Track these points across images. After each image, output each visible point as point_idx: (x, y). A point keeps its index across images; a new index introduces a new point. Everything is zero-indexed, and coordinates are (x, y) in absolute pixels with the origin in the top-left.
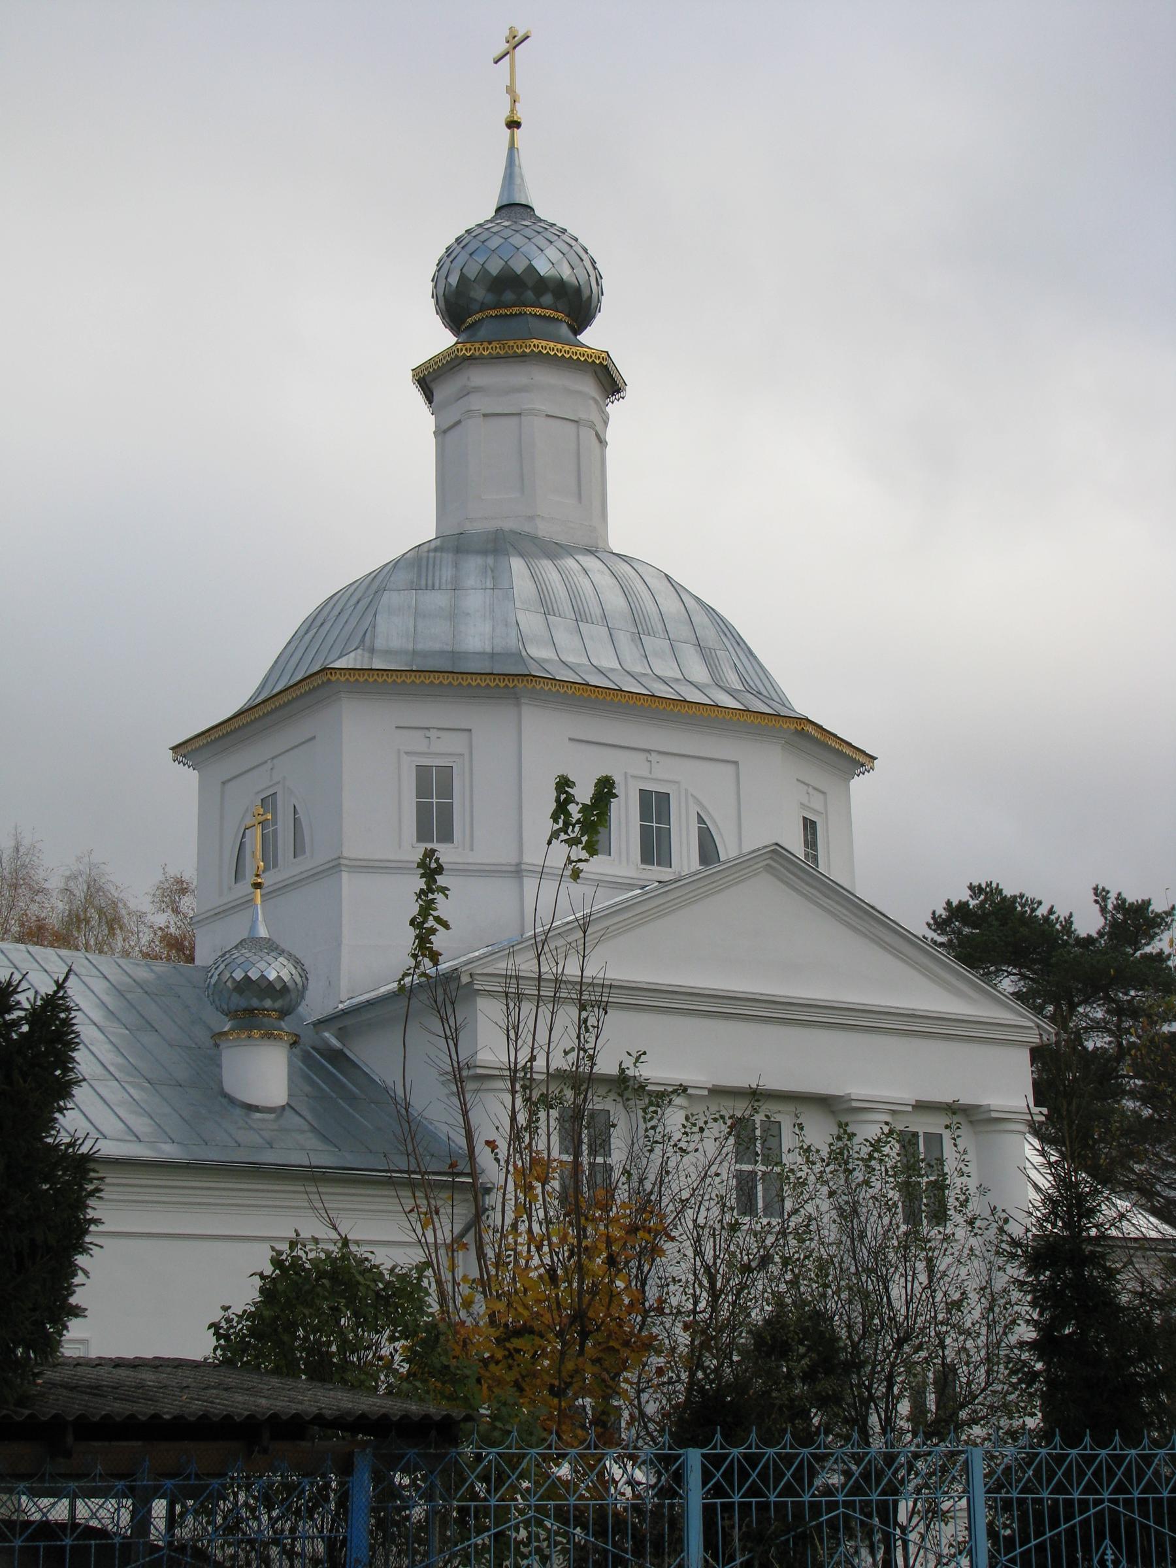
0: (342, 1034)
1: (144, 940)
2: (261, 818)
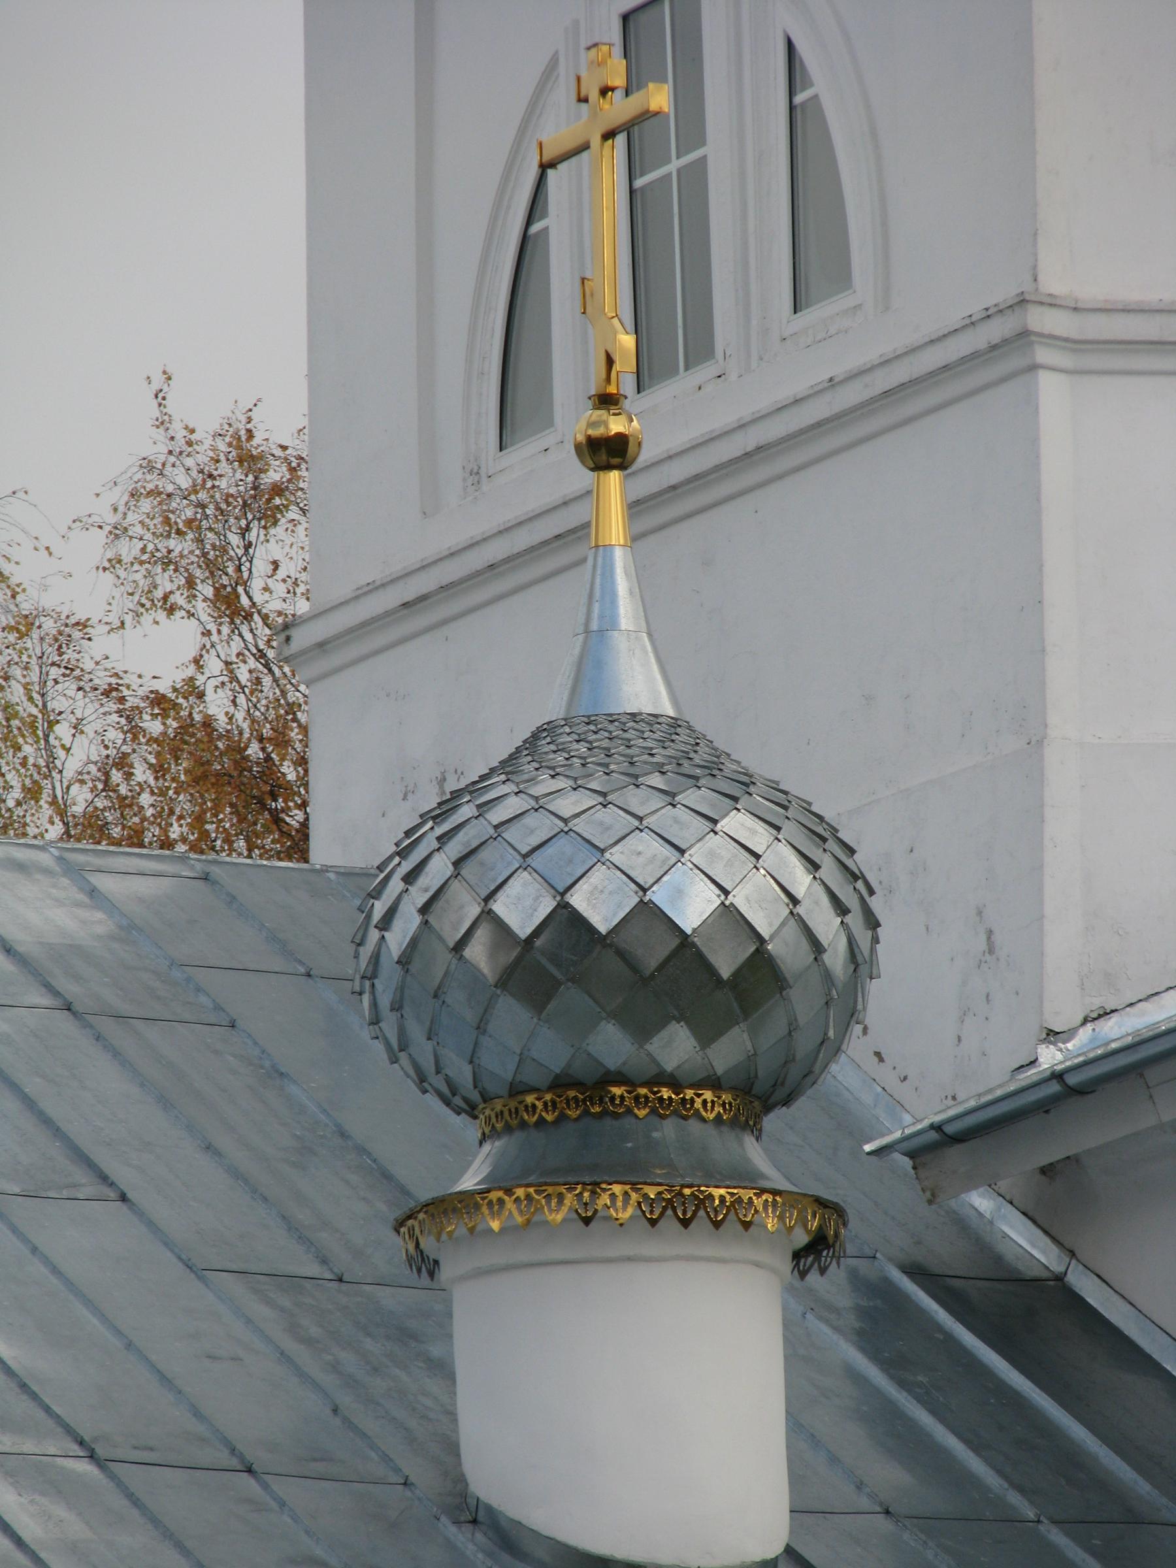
0: (1058, 1196)
1: (80, 755)
2: (619, 108)
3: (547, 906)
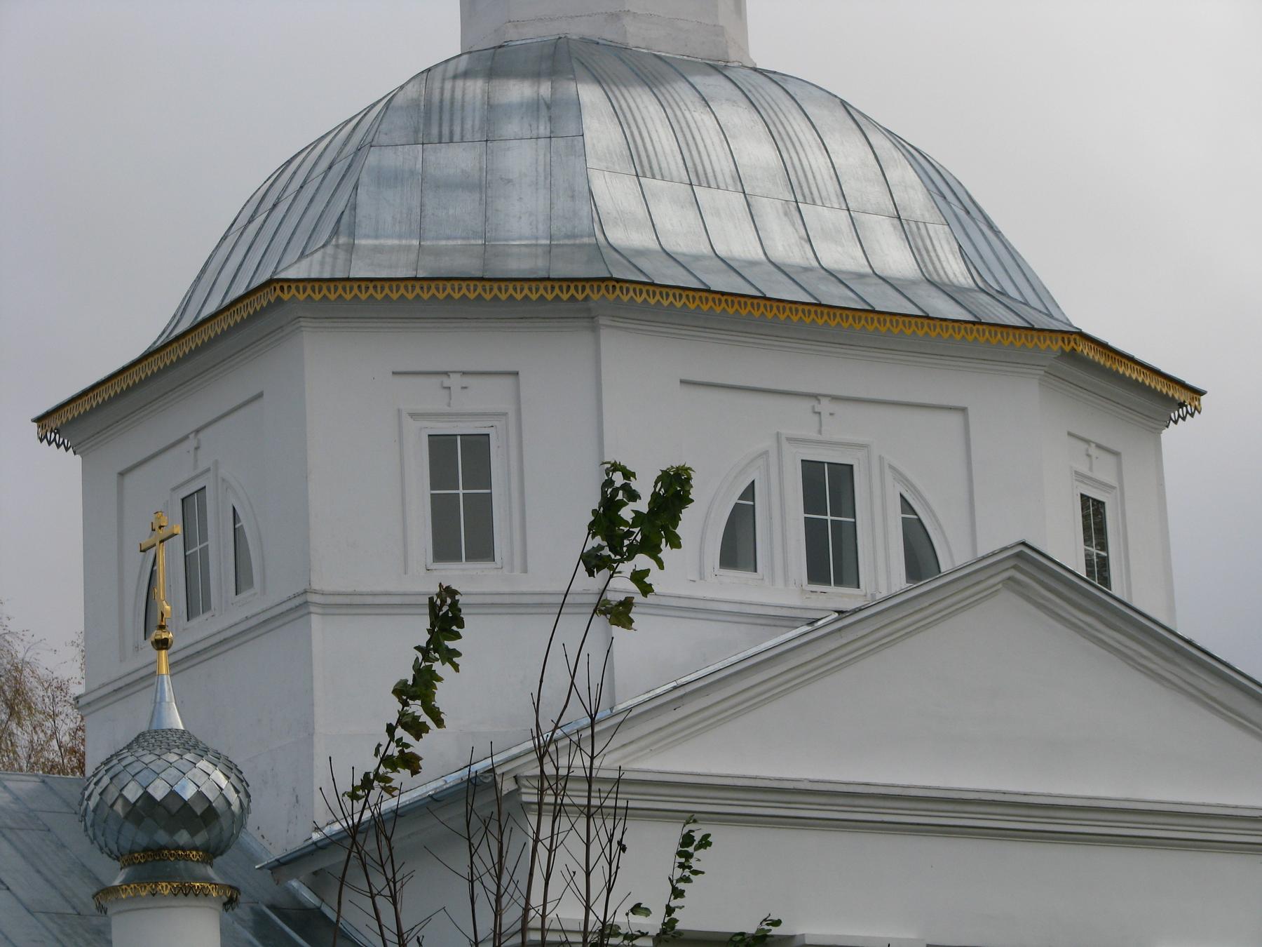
0: (317, 882)
3: (140, 792)
